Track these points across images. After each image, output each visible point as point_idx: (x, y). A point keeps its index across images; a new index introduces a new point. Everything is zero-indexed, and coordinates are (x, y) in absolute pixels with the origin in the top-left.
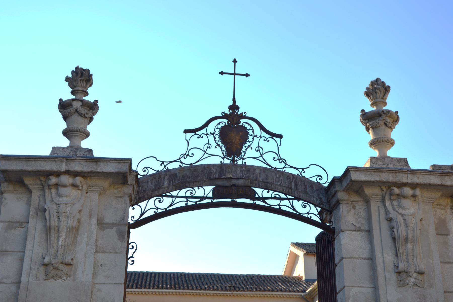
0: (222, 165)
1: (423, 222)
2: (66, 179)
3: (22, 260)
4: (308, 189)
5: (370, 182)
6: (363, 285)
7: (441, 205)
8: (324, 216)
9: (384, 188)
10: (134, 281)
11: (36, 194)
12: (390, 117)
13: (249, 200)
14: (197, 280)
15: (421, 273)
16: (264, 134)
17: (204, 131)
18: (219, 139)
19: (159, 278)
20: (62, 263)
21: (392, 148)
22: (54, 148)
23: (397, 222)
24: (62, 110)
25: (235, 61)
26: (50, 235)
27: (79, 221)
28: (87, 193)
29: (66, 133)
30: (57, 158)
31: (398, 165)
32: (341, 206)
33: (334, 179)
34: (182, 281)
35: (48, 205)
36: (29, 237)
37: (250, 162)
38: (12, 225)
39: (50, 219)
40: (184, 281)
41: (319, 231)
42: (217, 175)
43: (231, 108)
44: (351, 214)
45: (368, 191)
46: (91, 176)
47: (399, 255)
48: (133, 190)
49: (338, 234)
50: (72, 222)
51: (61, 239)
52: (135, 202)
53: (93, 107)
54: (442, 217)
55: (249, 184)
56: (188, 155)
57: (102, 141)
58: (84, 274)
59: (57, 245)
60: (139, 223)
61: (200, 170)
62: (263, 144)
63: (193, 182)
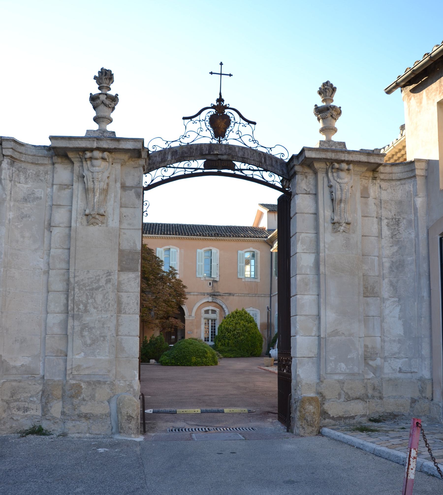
0: (211, 145)
1: (353, 188)
2: (97, 154)
3: (71, 211)
4: (274, 163)
5: (319, 159)
6: (309, 232)
7: (366, 177)
8: (285, 183)
9: (328, 164)
10: (147, 229)
11: (77, 165)
12: (335, 111)
13: (230, 171)
14: (192, 229)
15: (348, 224)
16: (242, 121)
17: (197, 118)
18: (209, 125)
19: (164, 228)
20: (98, 214)
21: (336, 134)
22: (88, 131)
23: (335, 188)
24: (92, 102)
25: (221, 64)
26: (88, 194)
27: (108, 184)
28: (112, 164)
29: (96, 119)
30: (90, 138)
31: (339, 147)
32: (297, 176)
33: (293, 157)
34: (181, 229)
35: (86, 173)
36: (74, 195)
37: (232, 142)
38: (63, 187)
39: (87, 183)
40: (182, 229)
41: (280, 194)
42: (207, 152)
43: (218, 100)
44: (304, 182)
45: (317, 165)
46: (115, 152)
47: (335, 211)
48: (146, 162)
49: (294, 196)
50: (103, 185)
51: (96, 197)
52: (148, 170)
53: (115, 99)
54: (366, 185)
55: (231, 159)
56: (185, 137)
57: (123, 125)
58: (113, 222)
59: (94, 202)
60: (150, 187)
61: (195, 148)
62: (241, 128)
63: (190, 157)
